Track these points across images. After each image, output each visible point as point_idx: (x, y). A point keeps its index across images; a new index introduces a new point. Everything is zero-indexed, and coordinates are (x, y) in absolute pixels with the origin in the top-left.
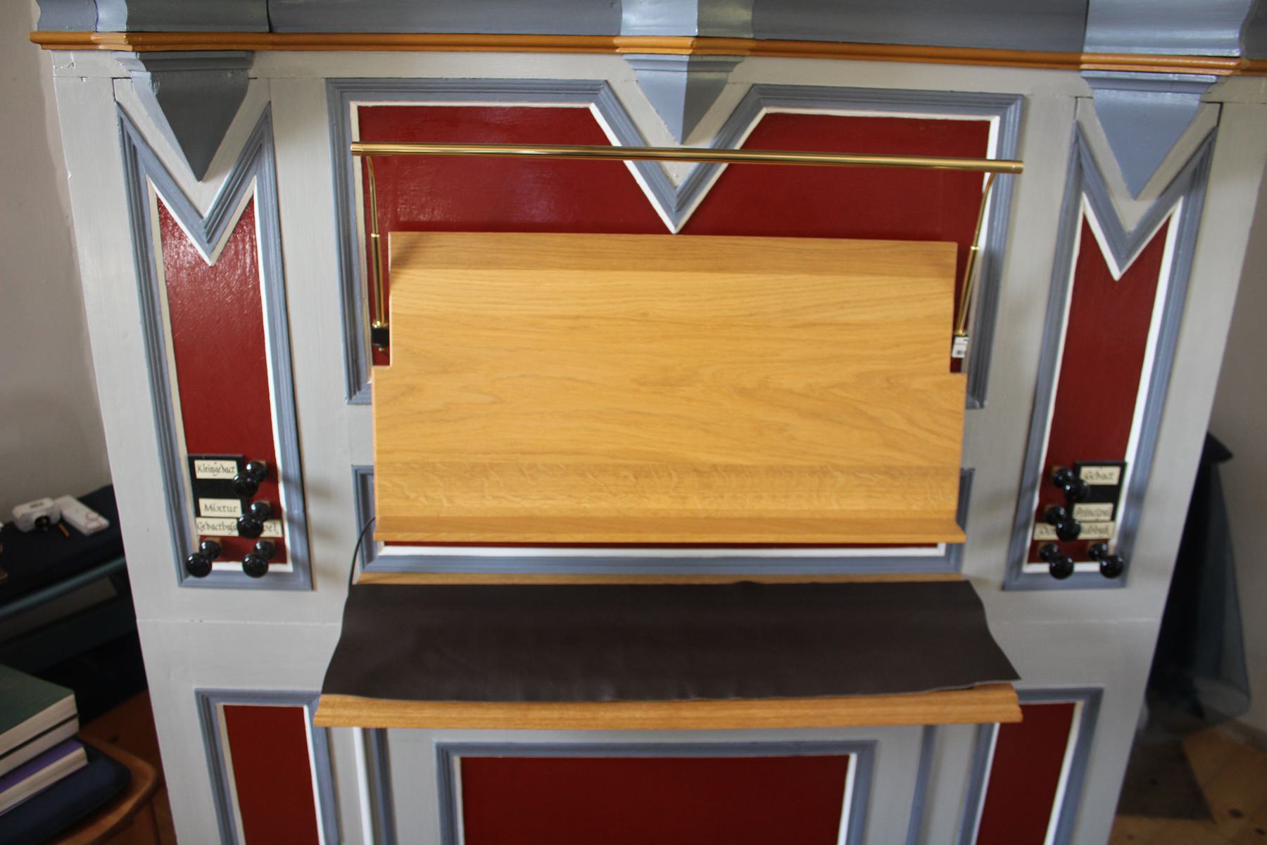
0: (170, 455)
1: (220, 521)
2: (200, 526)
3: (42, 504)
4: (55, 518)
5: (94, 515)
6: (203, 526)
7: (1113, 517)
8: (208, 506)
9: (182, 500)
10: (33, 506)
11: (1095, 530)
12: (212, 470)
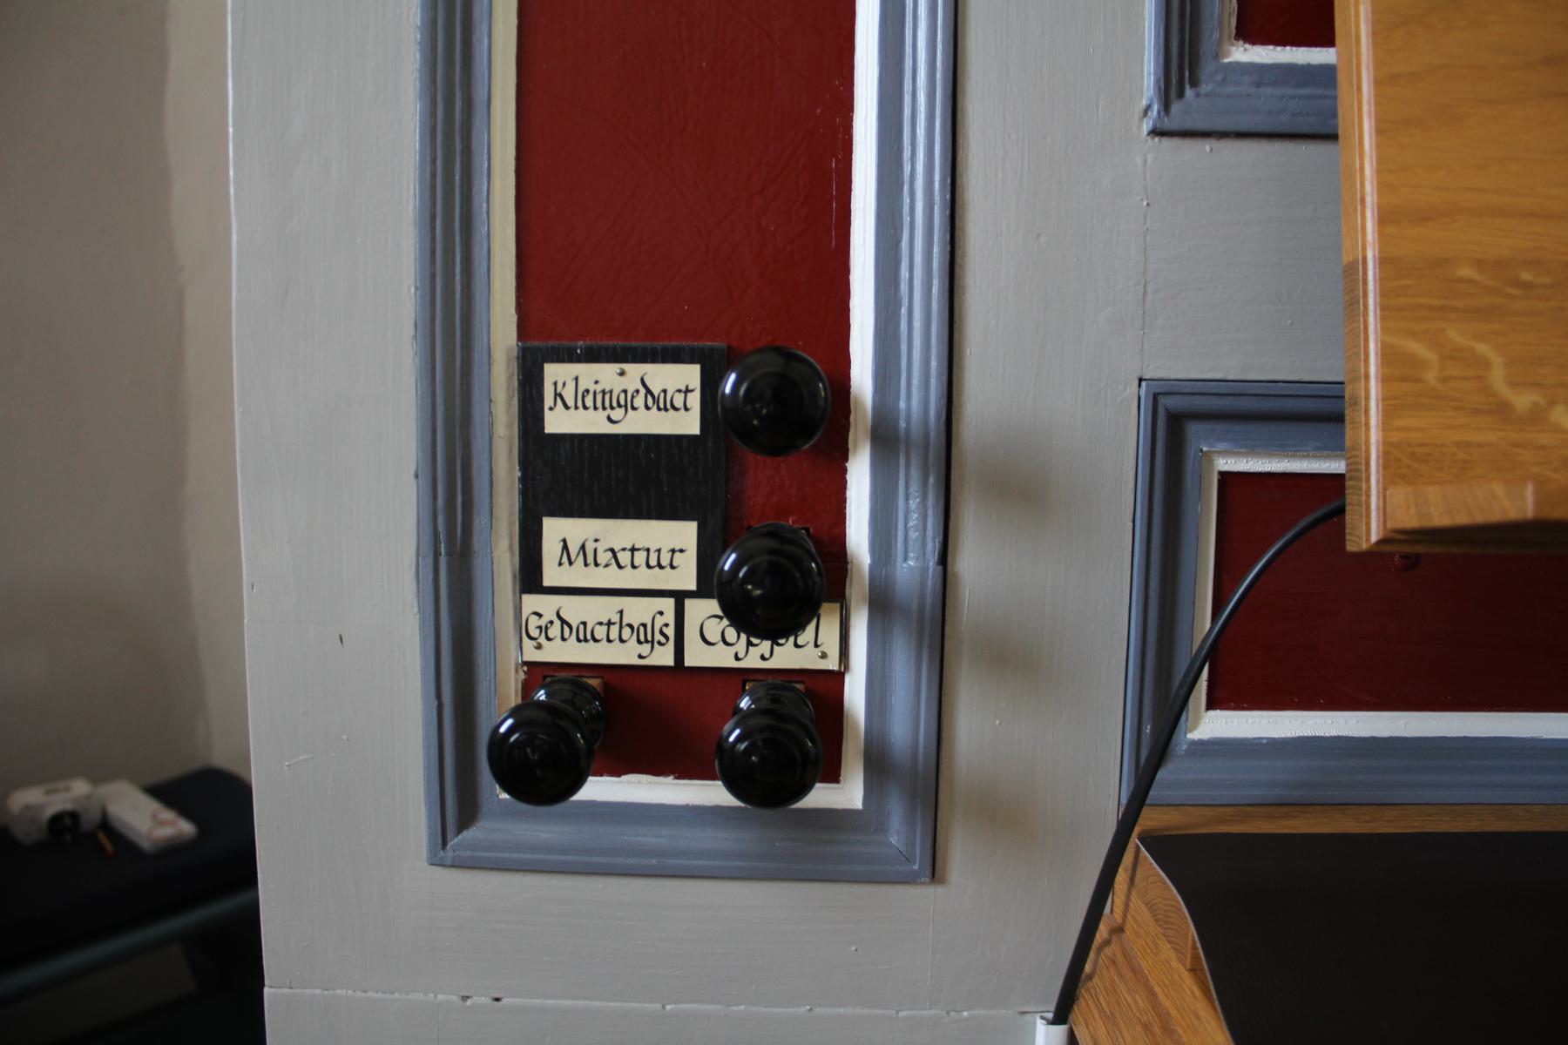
0: (458, 400)
1: (605, 608)
2: (534, 622)
3: (67, 789)
4: (90, 819)
5: (168, 815)
6: (544, 630)
8: (574, 549)
9: (480, 521)
10: (48, 792)
12: (605, 400)
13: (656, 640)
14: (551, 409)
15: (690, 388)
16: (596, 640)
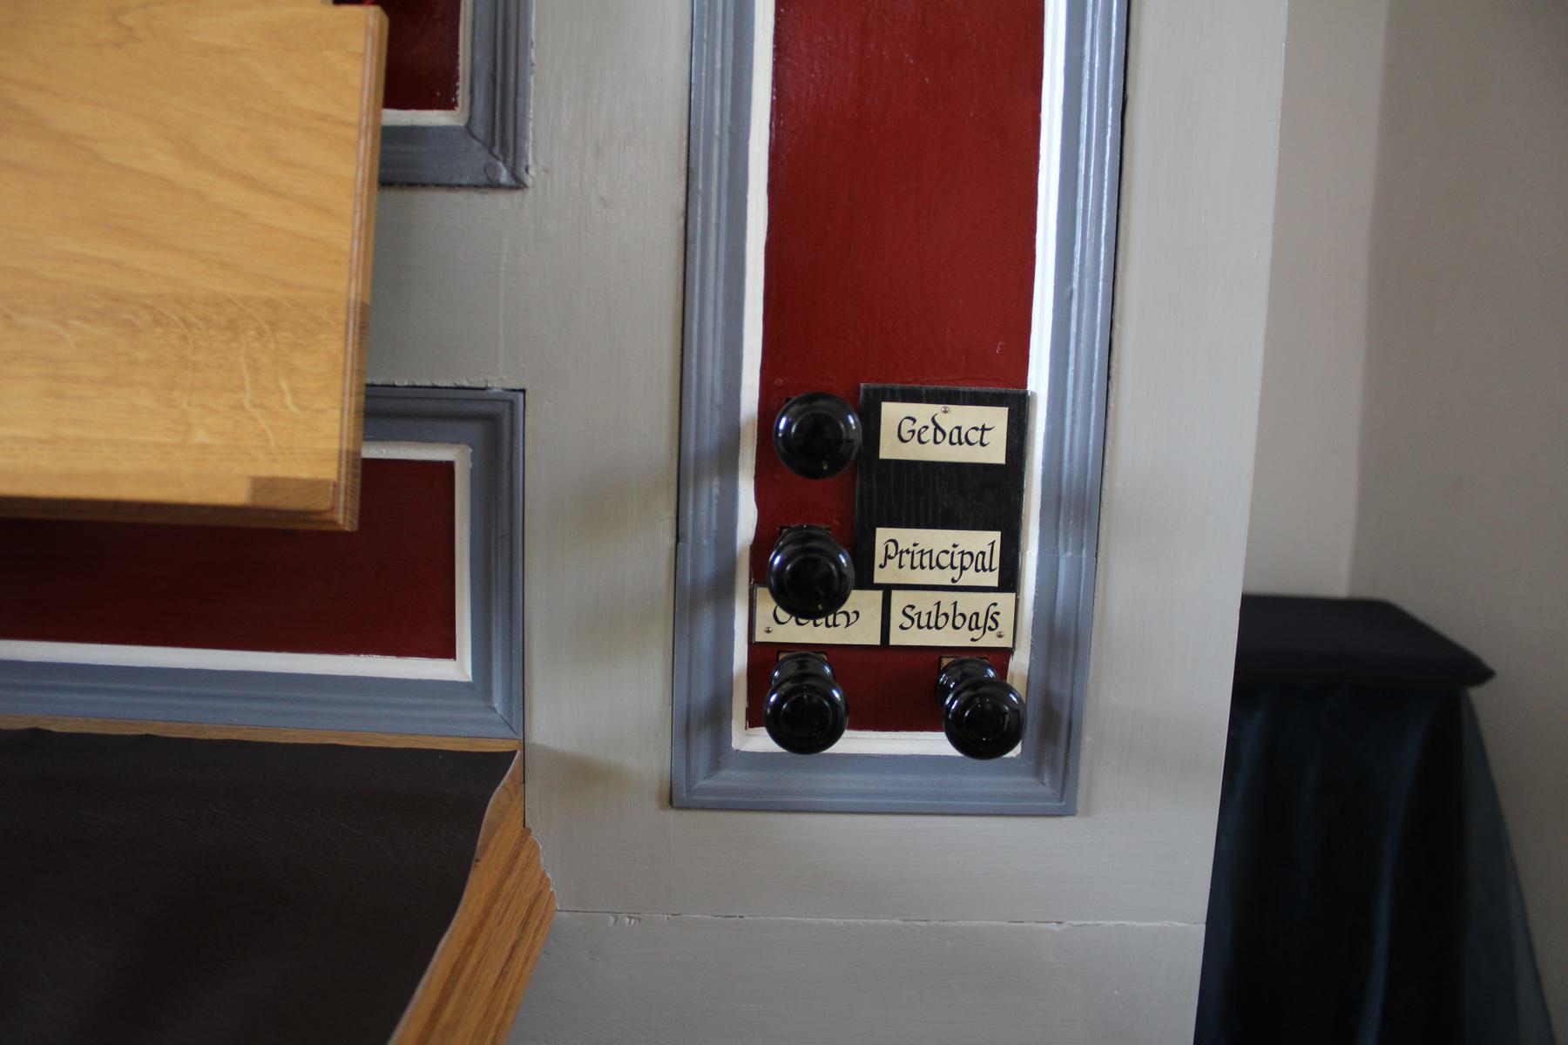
7: (1009, 580)
11: (955, 618)
13: (988, 626)
14: (881, 566)
15: (986, 427)
16: (970, 444)
